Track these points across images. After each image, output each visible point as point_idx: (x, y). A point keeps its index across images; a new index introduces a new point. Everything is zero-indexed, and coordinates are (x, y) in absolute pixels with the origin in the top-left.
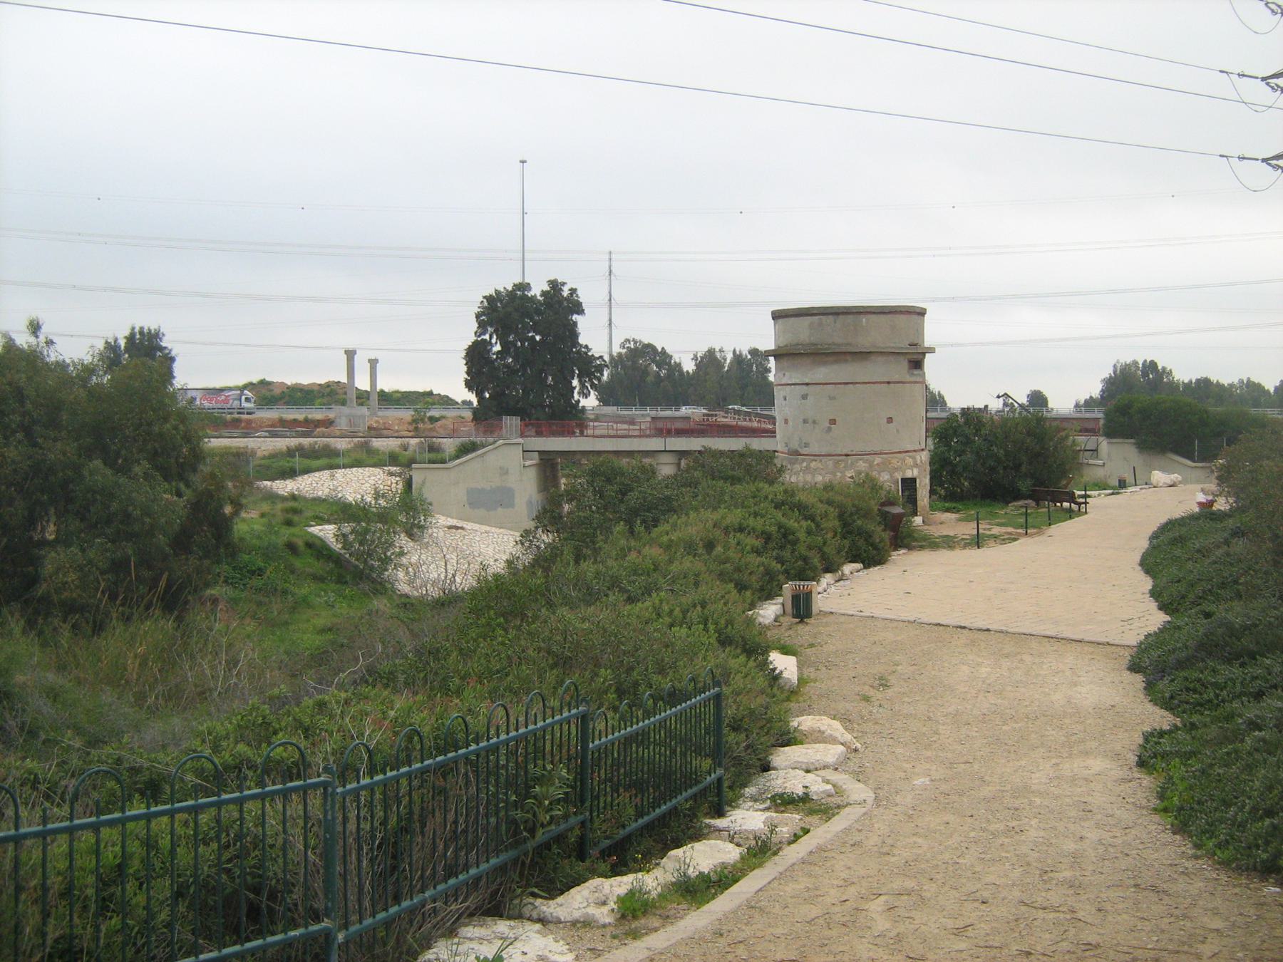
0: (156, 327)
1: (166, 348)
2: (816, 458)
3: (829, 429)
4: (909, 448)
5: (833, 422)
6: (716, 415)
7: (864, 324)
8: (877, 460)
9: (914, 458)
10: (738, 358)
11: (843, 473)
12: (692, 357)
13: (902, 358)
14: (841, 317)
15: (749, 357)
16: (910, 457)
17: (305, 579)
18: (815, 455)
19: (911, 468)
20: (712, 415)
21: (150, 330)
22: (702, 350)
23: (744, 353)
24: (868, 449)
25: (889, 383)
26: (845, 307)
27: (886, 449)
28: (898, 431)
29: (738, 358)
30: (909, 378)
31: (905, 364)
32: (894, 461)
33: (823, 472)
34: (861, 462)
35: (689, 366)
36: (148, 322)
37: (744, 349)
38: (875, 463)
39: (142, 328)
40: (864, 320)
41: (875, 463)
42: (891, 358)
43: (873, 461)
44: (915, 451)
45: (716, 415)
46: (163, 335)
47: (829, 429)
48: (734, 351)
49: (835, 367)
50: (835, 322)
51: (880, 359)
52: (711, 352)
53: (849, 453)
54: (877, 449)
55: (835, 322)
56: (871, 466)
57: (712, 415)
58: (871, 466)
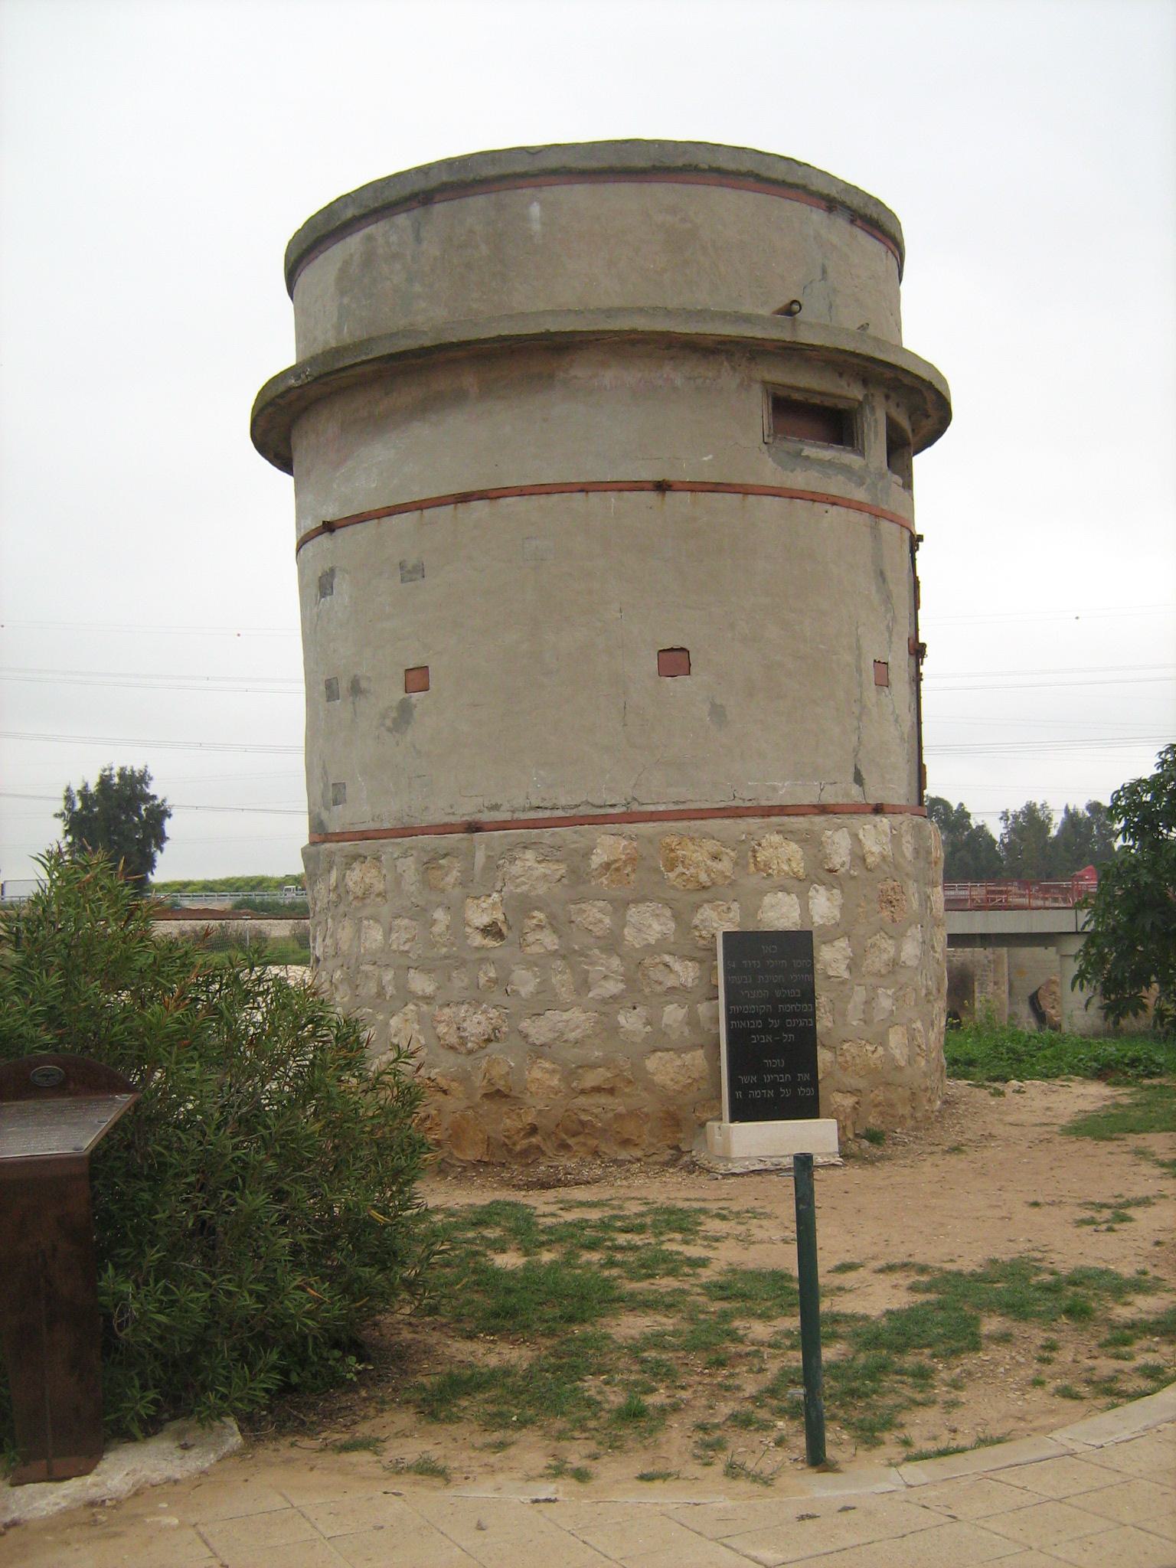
0: (142, 768)
1: (154, 797)
2: (363, 847)
3: (405, 711)
4: (786, 792)
5: (417, 678)
6: (1006, 892)
7: (537, 227)
8: (607, 846)
9: (810, 841)
10: (1072, 818)
11: (456, 910)
12: (1001, 815)
13: (727, 377)
14: (439, 209)
15: (1088, 814)
16: (788, 834)
17: (457, 1134)
18: (364, 836)
19: (800, 885)
20: (1001, 892)
21: (133, 772)
22: (1017, 806)
23: (1080, 811)
24: (566, 798)
25: (662, 487)
26: (449, 164)
27: (660, 794)
28: (718, 712)
29: (1071, 817)
30: (769, 472)
31: (757, 410)
32: (697, 855)
33: (385, 910)
34: (530, 855)
35: (997, 830)
36: (134, 762)
37: (1080, 806)
38: (597, 859)
39: (123, 769)
40: (535, 210)
41: (597, 859)
42: (676, 375)
43: (587, 854)
44: (823, 809)
45: (1006, 892)
46: (151, 779)
47: (405, 711)
48: (1067, 810)
49: (421, 431)
50: (418, 240)
51: (613, 376)
52: (1030, 811)
53: (487, 817)
54: (612, 795)
55: (418, 240)
56: (577, 875)
57: (1001, 892)
58: (577, 875)
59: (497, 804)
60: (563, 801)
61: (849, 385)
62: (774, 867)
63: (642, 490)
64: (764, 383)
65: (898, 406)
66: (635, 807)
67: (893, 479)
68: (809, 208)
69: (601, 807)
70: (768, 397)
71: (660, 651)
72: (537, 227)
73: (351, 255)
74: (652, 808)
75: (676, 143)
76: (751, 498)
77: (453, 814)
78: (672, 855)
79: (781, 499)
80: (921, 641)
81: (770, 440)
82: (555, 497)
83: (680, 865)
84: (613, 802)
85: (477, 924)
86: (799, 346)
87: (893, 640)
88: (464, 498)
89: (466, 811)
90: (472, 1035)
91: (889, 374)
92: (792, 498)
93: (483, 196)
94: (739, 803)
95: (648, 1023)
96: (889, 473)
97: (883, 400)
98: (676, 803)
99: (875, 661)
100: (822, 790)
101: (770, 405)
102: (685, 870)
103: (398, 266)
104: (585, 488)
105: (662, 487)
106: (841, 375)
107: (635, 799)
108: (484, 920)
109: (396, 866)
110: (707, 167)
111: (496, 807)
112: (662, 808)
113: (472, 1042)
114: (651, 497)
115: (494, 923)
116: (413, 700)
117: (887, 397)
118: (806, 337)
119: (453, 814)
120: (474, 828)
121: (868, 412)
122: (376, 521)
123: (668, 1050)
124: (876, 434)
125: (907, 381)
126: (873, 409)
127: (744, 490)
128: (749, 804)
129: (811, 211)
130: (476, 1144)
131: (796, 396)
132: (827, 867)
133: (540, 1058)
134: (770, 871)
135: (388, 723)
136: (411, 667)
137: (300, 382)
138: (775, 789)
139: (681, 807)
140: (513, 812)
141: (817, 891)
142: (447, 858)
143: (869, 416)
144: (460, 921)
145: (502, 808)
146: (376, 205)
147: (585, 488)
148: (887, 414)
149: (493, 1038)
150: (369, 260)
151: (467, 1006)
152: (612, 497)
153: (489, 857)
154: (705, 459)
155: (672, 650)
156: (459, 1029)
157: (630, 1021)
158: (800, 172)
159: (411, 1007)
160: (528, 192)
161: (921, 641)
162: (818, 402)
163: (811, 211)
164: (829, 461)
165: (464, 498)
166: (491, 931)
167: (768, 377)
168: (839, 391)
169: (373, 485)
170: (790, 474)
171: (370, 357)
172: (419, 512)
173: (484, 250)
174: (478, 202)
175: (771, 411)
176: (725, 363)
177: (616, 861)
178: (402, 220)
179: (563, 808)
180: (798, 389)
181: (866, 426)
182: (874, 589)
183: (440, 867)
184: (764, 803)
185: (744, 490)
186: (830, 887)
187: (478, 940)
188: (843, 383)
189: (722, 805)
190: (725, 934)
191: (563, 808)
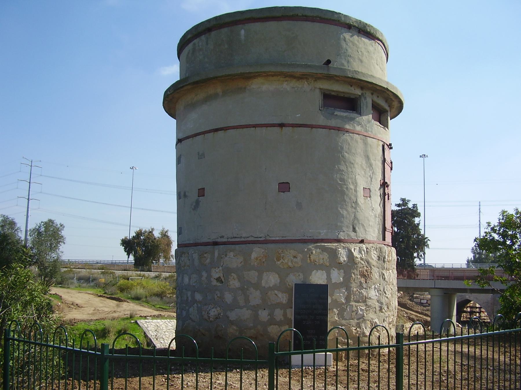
3: (197, 203)
7: (243, 38)
14: (213, 33)
19: (327, 269)
25: (281, 125)
30: (321, 120)
40: (243, 32)
47: (197, 203)
50: (207, 44)
53: (219, 240)
55: (207, 44)
59: (223, 236)
60: (244, 235)
61: (355, 89)
62: (317, 261)
63: (274, 126)
64: (320, 89)
65: (378, 97)
66: (268, 238)
67: (375, 123)
68: (341, 28)
69: (257, 238)
70: (322, 93)
71: (279, 183)
72: (243, 38)
73: (190, 50)
74: (274, 239)
75: (290, 7)
76: (314, 129)
77: (210, 239)
78: (279, 255)
79: (326, 129)
80: (386, 181)
81: (322, 109)
82: (245, 129)
83: (282, 259)
84: (261, 236)
85: (215, 277)
86: (331, 76)
87: (372, 180)
88: (216, 130)
89: (213, 238)
90: (212, 316)
91: (370, 86)
92: (330, 129)
93: (226, 28)
94: (306, 238)
95: (269, 315)
96: (373, 121)
97: (370, 95)
98: (283, 237)
99: (364, 188)
100: (339, 234)
101: (322, 96)
102: (283, 261)
103: (201, 53)
104: (255, 126)
105: (281, 125)
106: (351, 86)
107: (268, 235)
108: (217, 276)
109: (193, 256)
110: (301, 15)
111: (222, 237)
112: (278, 238)
113: (212, 318)
114: (277, 129)
115: (220, 277)
116: (200, 199)
117: (372, 94)
118: (332, 72)
119: (210, 239)
120: (215, 244)
121: (363, 99)
122: (192, 138)
123: (275, 325)
124: (367, 107)
125: (378, 88)
126: (365, 98)
127: (312, 127)
128: (310, 238)
129: (342, 29)
130: (77, 329)
131: (333, 93)
132: (338, 262)
133: (233, 325)
134: (316, 263)
135: (193, 207)
136: (200, 188)
137: (170, 93)
138: (320, 233)
139: (284, 239)
140: (228, 239)
141: (334, 270)
142: (207, 254)
143: (363, 100)
144: (209, 276)
145: (225, 237)
146: (196, 33)
147: (255, 126)
148: (372, 100)
149: (218, 317)
150: (194, 50)
151: (211, 305)
152: (264, 129)
153: (219, 254)
154: (297, 116)
155: (283, 183)
156: (208, 313)
157: (264, 315)
158: (336, 16)
159: (195, 305)
160: (240, 26)
161: (386, 181)
162: (342, 95)
163: (342, 29)
164: (345, 116)
165: (216, 130)
166: (219, 280)
167: (321, 87)
168: (351, 92)
169: (192, 127)
170: (330, 121)
171: (187, 83)
172: (203, 135)
173: (226, 46)
174: (225, 30)
175: (322, 99)
176: (306, 82)
177: (259, 257)
178: (203, 37)
179: (244, 238)
180: (334, 91)
181: (362, 104)
182: (364, 162)
183: (205, 257)
184: (315, 238)
185: (312, 127)
186: (339, 269)
187: (215, 283)
188: (352, 88)
189: (300, 238)
190: (295, 284)
191: (244, 238)
